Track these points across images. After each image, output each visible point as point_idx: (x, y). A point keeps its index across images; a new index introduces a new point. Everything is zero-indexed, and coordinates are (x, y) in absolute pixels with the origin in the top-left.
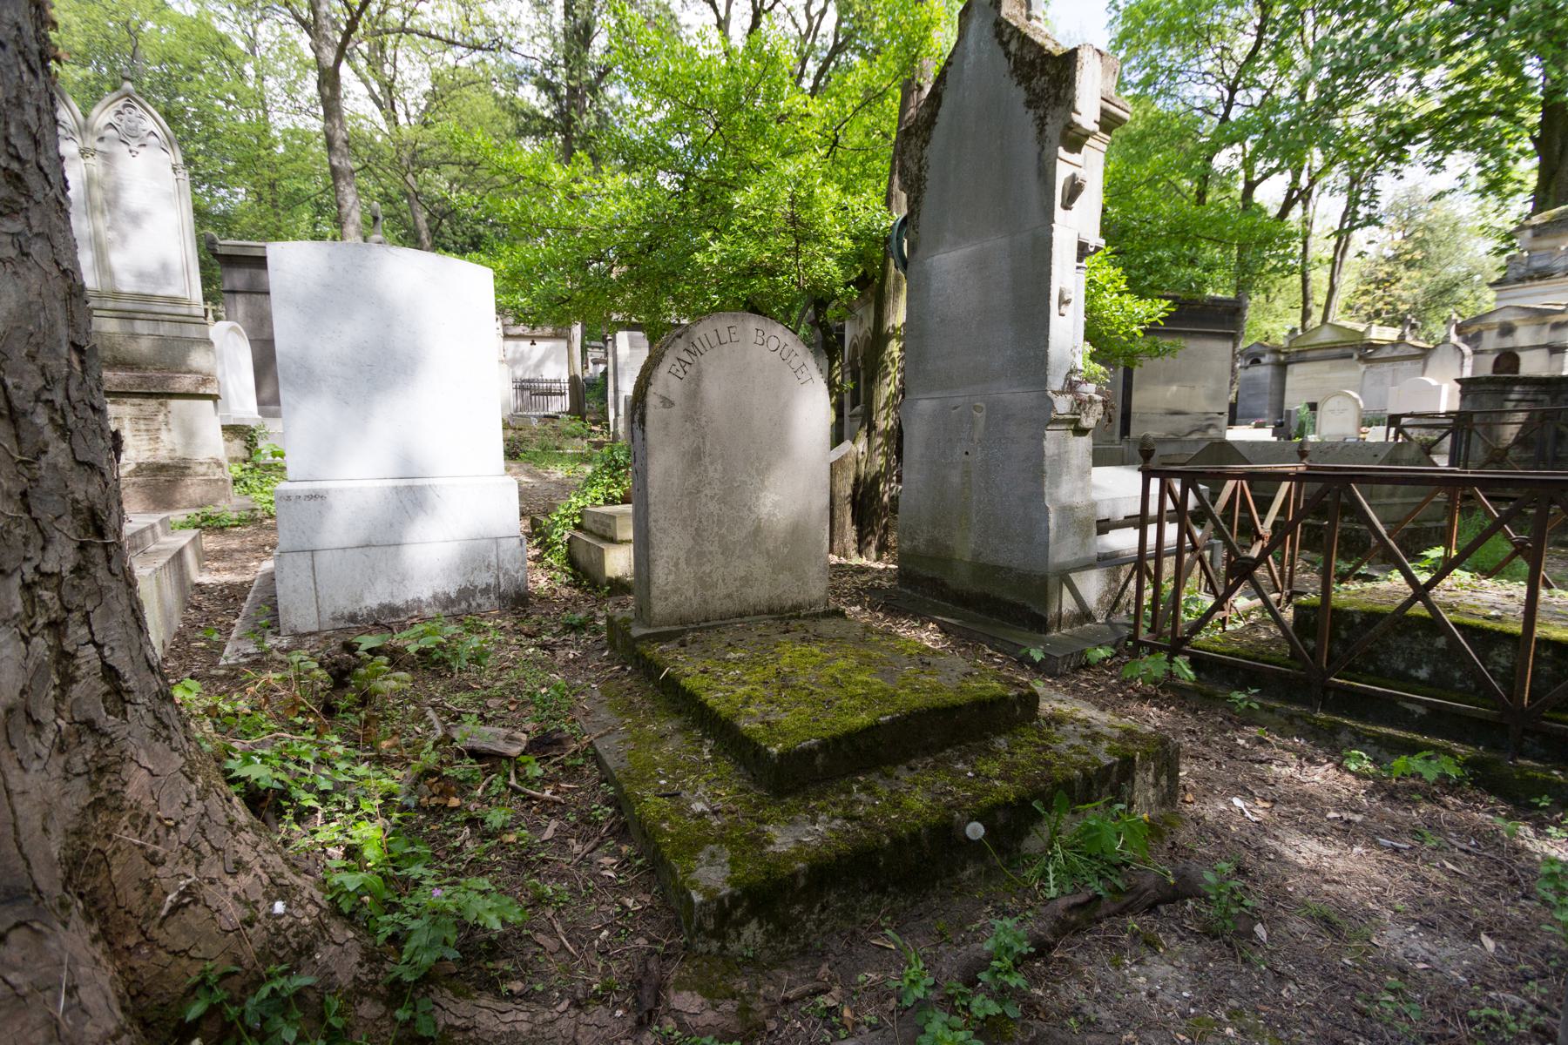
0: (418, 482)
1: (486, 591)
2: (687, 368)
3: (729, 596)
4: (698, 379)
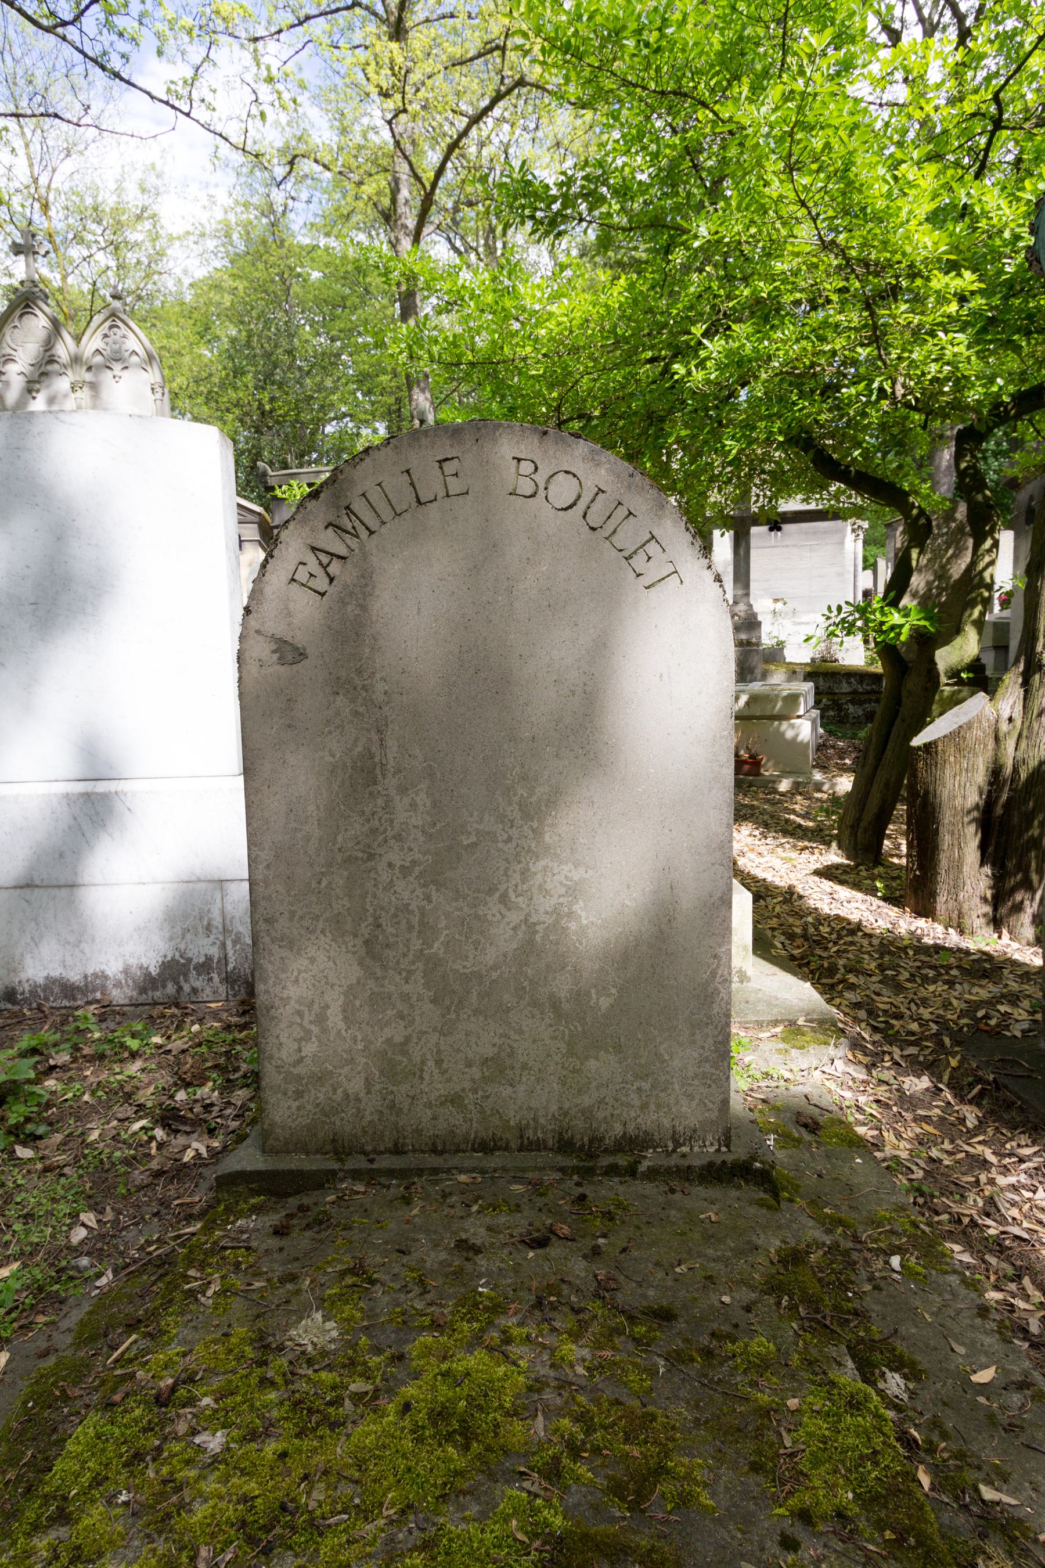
0: (101, 787)
1: (205, 967)
2: (335, 568)
3: (455, 1100)
4: (362, 591)
